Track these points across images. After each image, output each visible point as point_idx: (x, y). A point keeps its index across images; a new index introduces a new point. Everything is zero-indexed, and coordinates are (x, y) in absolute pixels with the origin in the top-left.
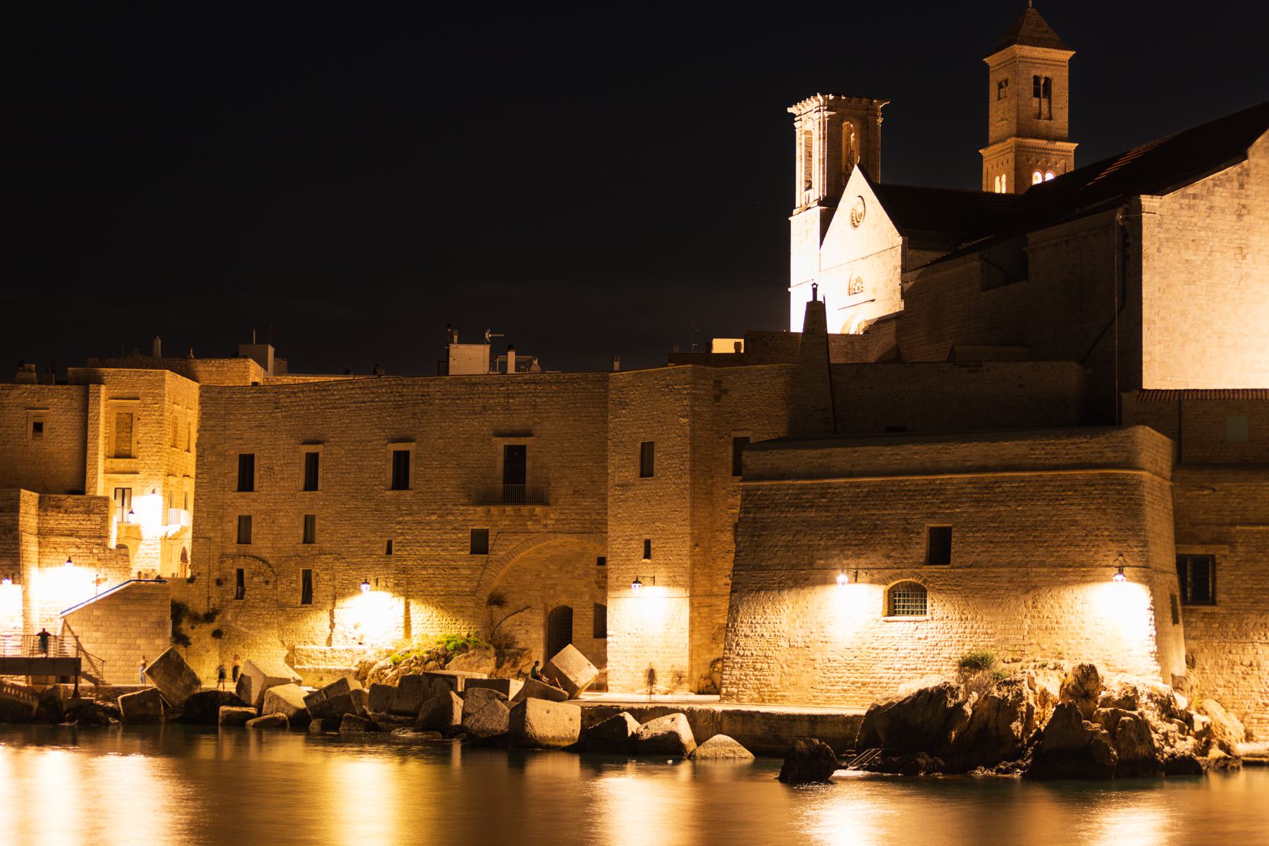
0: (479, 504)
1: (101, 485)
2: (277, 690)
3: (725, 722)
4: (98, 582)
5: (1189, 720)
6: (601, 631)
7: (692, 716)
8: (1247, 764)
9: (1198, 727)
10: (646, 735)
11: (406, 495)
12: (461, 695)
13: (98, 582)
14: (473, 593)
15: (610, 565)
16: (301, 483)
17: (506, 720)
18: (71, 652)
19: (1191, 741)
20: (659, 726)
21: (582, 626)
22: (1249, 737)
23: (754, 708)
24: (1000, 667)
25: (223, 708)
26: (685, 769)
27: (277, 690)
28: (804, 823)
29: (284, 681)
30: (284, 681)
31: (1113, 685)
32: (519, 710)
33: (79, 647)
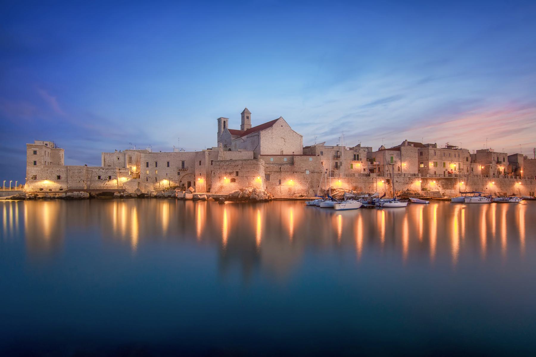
0: (207, 173)
1: (128, 167)
2: (152, 193)
3: (211, 196)
4: (128, 179)
5: (267, 195)
6: (195, 185)
7: (207, 195)
8: (274, 200)
9: (268, 195)
10: (201, 198)
11: (169, 168)
12: (177, 193)
13: (128, 179)
14: (178, 180)
15: (196, 176)
16: (155, 166)
17: (89, 195)
18: (124, 188)
19: (267, 197)
20: (202, 197)
21: (192, 184)
22: (273, 197)
23: (214, 194)
24: (138, 179)
25: (145, 195)
26: (206, 202)
27: (152, 193)
28: (429, 187)
29: (154, 192)
30: (154, 192)
31: (258, 190)
32: (185, 195)
33: (125, 188)
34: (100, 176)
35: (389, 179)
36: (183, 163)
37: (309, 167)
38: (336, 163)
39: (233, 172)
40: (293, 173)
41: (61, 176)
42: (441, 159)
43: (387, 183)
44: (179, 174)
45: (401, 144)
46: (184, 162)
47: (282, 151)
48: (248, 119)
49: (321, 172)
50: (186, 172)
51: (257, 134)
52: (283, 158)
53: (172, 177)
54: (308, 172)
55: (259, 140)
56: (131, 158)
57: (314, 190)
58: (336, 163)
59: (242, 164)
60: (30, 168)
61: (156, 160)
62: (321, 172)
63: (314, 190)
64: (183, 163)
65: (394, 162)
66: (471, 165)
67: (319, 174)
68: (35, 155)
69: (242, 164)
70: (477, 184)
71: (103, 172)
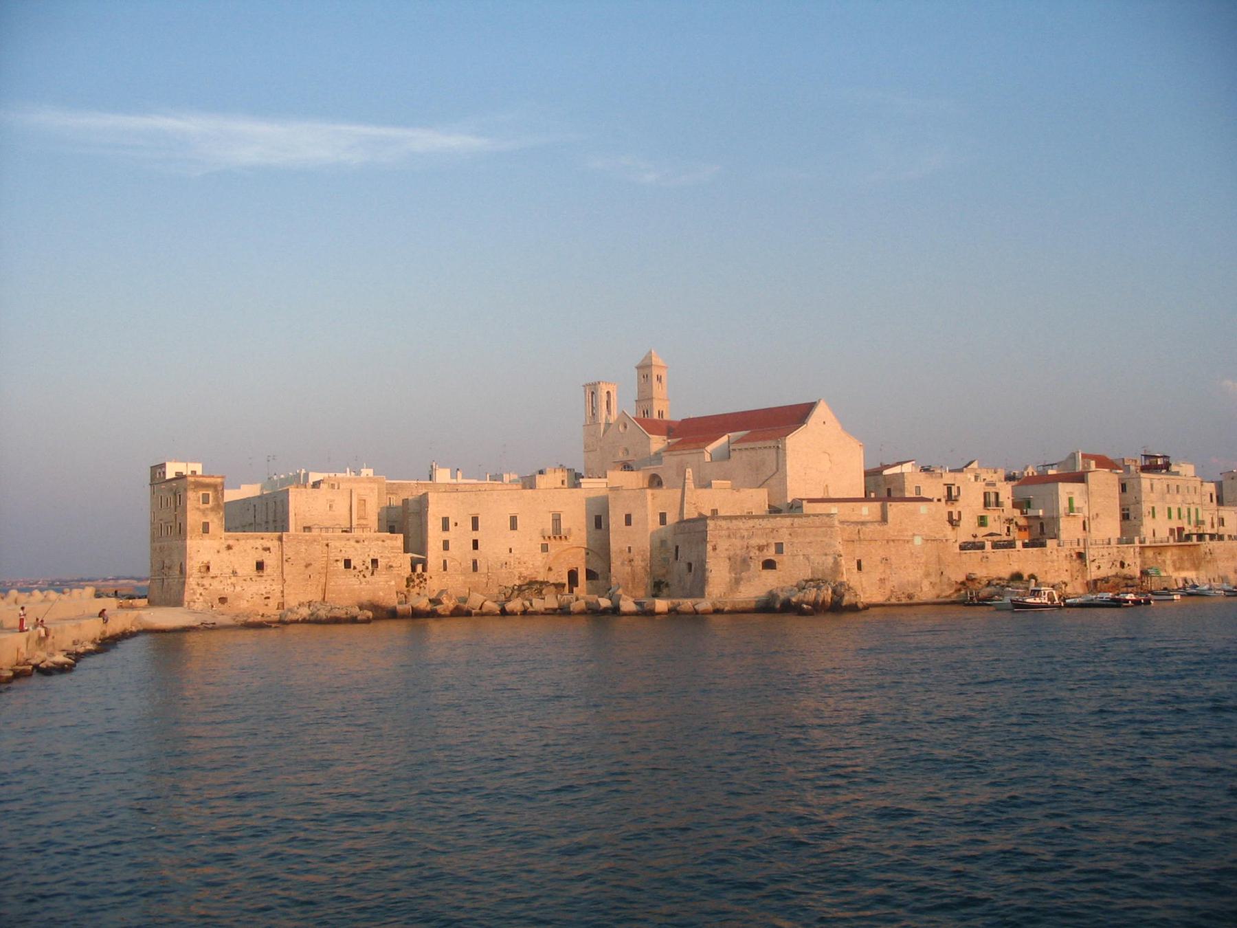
11: (515, 532)
34: (350, 560)
35: (1082, 551)
36: (557, 520)
37: (920, 528)
38: (950, 514)
39: (767, 545)
40: (888, 542)
41: (266, 562)
42: (1163, 499)
43: (1078, 561)
44: (545, 548)
45: (1064, 459)
46: (560, 515)
47: (827, 486)
48: (660, 382)
49: (947, 540)
50: (564, 542)
51: (771, 443)
52: (861, 509)
53: (526, 559)
54: (918, 541)
55: (780, 460)
56: (1078, 545)
57: (931, 583)
58: (950, 514)
59: (792, 524)
60: (194, 542)
61: (473, 511)
62: (947, 540)
63: (931, 583)
64: (557, 520)
65: (1075, 510)
66: (1218, 510)
67: (941, 545)
68: (445, 515)
69: (792, 524)
70: (795, 540)
71: (356, 549)
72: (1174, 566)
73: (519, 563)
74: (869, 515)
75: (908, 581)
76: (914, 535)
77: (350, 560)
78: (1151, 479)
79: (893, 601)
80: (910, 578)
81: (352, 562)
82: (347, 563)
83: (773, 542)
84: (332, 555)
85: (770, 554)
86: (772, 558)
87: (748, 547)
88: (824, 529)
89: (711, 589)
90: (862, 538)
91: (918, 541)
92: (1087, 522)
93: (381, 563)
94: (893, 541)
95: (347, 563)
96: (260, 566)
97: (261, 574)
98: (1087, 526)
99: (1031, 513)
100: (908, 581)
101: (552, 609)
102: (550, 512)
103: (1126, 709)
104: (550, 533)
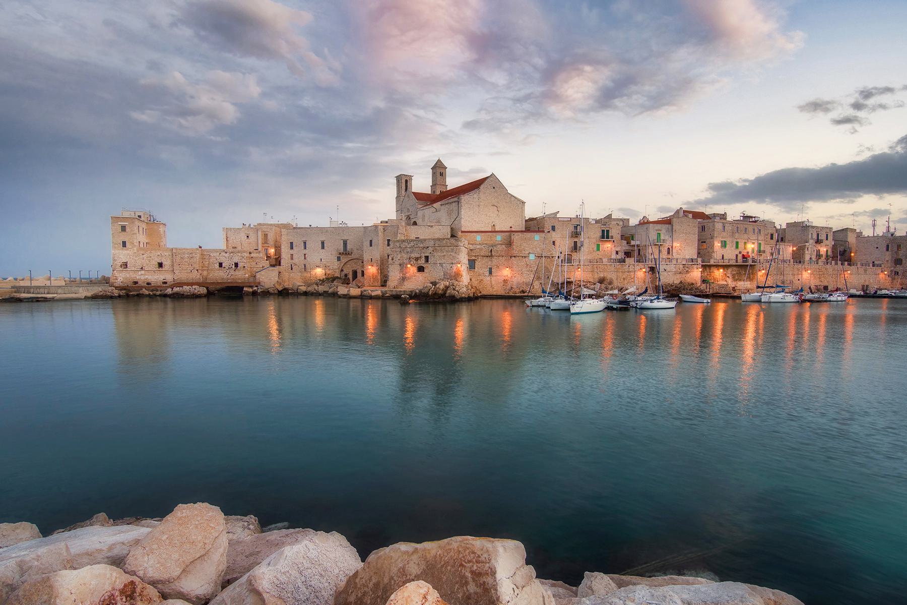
34: (222, 263)
35: (654, 266)
39: (420, 257)
44: (339, 259)
51: (456, 199)
54: (532, 257)
65: (661, 241)
72: (734, 277)
73: (325, 266)
74: (501, 241)
75: (523, 282)
76: (530, 253)
77: (222, 263)
78: (723, 223)
79: (511, 294)
80: (524, 280)
81: (829, 287)
82: (221, 265)
83: (423, 255)
84: (211, 260)
85: (422, 262)
86: (422, 265)
87: (410, 259)
88: (452, 247)
89: (390, 283)
90: (493, 255)
91: (532, 257)
92: (671, 249)
93: (240, 265)
94: (514, 256)
95: (221, 265)
96: (160, 265)
97: (161, 269)
98: (671, 251)
99: (633, 243)
100: (523, 282)
101: (344, 295)
102: (598, 246)
103: (236, 348)
104: (342, 251)
